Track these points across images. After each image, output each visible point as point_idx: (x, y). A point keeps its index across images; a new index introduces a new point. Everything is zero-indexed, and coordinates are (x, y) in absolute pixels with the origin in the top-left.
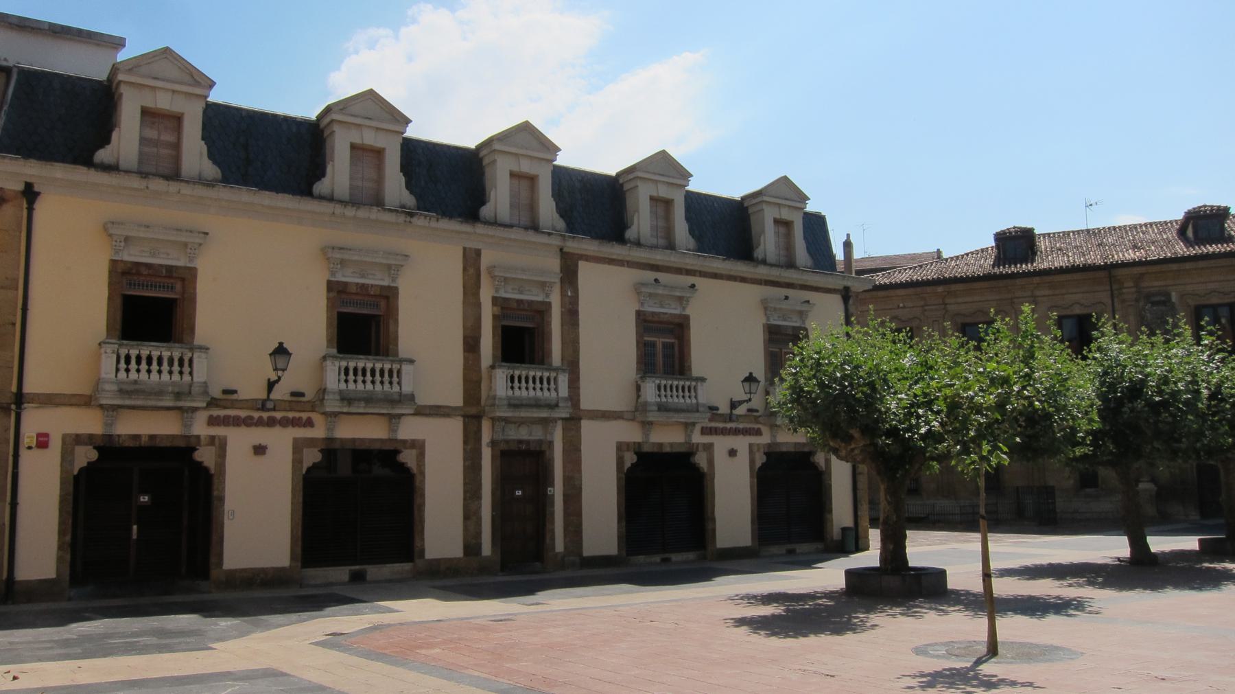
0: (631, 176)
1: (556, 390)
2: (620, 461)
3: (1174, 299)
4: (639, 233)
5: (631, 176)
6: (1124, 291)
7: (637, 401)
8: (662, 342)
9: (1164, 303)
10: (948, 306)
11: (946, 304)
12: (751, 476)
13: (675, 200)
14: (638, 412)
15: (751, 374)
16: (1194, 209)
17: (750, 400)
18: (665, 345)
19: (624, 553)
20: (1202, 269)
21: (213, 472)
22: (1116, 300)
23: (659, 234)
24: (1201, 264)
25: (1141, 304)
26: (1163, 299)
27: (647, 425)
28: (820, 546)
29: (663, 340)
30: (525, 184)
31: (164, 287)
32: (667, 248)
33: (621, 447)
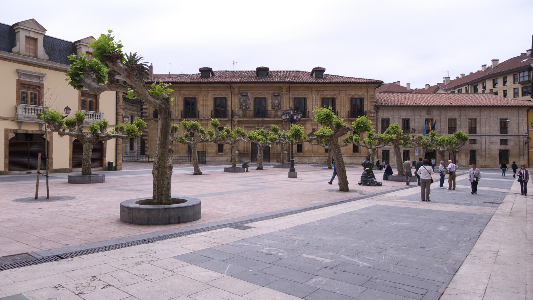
0: (17, 27)
1: (100, 119)
2: (6, 136)
3: (249, 95)
4: (19, 50)
5: (17, 27)
6: (235, 91)
7: (16, 114)
8: (30, 92)
9: (246, 96)
10: (181, 91)
11: (180, 91)
12: (70, 144)
13: (38, 40)
14: (15, 119)
15: (67, 106)
16: (259, 67)
17: (67, 116)
18: (90, 102)
19: (72, 167)
20: (257, 86)
21: (49, 141)
22: (232, 94)
23: (31, 51)
24: (257, 85)
25: (240, 95)
26: (246, 94)
27: (20, 123)
28: (101, 168)
29: (31, 92)
30: (32, 42)
31: (32, 88)
32: (34, 57)
33: (7, 131)
